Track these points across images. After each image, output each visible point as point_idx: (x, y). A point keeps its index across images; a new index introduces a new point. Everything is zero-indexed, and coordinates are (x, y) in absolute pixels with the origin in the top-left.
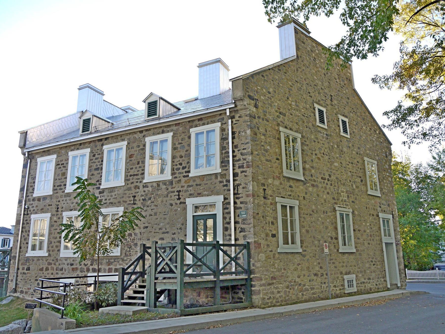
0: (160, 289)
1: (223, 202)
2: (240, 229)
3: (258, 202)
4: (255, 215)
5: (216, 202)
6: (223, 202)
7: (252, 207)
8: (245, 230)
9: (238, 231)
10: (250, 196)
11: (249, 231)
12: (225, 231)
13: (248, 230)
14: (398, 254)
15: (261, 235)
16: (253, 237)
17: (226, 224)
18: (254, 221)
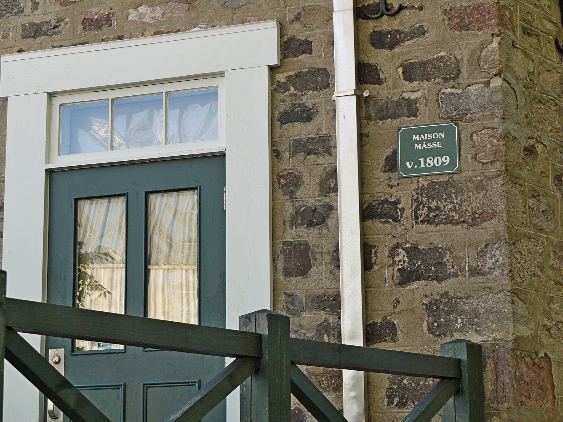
0: (363, 21)
1: (272, 69)
2: (401, 255)
3: (531, 74)
4: (517, 155)
5: (221, 74)
6: (272, 69)
7: (499, 96)
8: (440, 265)
9: (387, 273)
10: (482, 24)
11: (475, 272)
12: (287, 274)
13: (471, 261)
14: (368, 273)
15: (551, 300)
16: (507, 309)
17: (294, 224)
18: (508, 196)
